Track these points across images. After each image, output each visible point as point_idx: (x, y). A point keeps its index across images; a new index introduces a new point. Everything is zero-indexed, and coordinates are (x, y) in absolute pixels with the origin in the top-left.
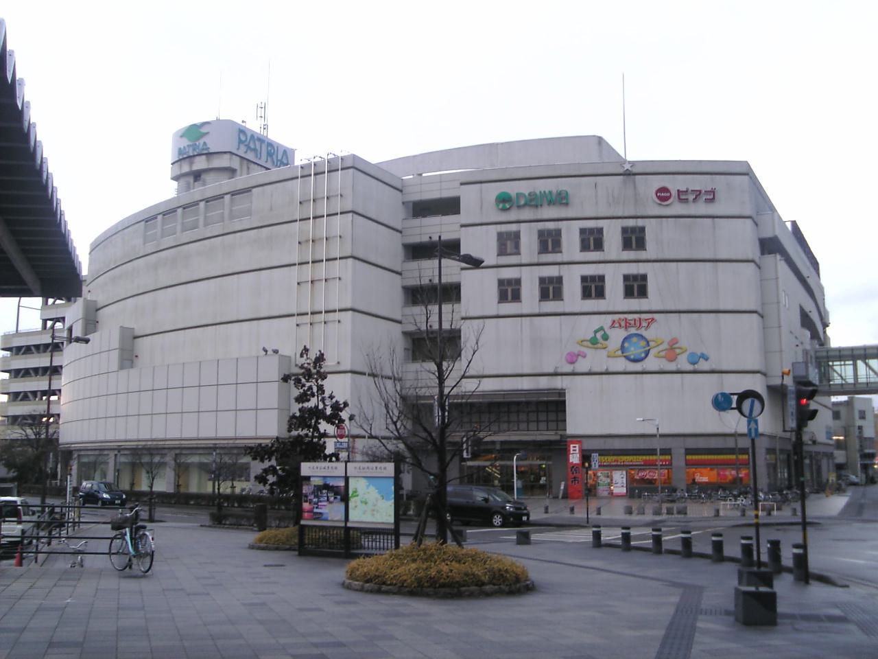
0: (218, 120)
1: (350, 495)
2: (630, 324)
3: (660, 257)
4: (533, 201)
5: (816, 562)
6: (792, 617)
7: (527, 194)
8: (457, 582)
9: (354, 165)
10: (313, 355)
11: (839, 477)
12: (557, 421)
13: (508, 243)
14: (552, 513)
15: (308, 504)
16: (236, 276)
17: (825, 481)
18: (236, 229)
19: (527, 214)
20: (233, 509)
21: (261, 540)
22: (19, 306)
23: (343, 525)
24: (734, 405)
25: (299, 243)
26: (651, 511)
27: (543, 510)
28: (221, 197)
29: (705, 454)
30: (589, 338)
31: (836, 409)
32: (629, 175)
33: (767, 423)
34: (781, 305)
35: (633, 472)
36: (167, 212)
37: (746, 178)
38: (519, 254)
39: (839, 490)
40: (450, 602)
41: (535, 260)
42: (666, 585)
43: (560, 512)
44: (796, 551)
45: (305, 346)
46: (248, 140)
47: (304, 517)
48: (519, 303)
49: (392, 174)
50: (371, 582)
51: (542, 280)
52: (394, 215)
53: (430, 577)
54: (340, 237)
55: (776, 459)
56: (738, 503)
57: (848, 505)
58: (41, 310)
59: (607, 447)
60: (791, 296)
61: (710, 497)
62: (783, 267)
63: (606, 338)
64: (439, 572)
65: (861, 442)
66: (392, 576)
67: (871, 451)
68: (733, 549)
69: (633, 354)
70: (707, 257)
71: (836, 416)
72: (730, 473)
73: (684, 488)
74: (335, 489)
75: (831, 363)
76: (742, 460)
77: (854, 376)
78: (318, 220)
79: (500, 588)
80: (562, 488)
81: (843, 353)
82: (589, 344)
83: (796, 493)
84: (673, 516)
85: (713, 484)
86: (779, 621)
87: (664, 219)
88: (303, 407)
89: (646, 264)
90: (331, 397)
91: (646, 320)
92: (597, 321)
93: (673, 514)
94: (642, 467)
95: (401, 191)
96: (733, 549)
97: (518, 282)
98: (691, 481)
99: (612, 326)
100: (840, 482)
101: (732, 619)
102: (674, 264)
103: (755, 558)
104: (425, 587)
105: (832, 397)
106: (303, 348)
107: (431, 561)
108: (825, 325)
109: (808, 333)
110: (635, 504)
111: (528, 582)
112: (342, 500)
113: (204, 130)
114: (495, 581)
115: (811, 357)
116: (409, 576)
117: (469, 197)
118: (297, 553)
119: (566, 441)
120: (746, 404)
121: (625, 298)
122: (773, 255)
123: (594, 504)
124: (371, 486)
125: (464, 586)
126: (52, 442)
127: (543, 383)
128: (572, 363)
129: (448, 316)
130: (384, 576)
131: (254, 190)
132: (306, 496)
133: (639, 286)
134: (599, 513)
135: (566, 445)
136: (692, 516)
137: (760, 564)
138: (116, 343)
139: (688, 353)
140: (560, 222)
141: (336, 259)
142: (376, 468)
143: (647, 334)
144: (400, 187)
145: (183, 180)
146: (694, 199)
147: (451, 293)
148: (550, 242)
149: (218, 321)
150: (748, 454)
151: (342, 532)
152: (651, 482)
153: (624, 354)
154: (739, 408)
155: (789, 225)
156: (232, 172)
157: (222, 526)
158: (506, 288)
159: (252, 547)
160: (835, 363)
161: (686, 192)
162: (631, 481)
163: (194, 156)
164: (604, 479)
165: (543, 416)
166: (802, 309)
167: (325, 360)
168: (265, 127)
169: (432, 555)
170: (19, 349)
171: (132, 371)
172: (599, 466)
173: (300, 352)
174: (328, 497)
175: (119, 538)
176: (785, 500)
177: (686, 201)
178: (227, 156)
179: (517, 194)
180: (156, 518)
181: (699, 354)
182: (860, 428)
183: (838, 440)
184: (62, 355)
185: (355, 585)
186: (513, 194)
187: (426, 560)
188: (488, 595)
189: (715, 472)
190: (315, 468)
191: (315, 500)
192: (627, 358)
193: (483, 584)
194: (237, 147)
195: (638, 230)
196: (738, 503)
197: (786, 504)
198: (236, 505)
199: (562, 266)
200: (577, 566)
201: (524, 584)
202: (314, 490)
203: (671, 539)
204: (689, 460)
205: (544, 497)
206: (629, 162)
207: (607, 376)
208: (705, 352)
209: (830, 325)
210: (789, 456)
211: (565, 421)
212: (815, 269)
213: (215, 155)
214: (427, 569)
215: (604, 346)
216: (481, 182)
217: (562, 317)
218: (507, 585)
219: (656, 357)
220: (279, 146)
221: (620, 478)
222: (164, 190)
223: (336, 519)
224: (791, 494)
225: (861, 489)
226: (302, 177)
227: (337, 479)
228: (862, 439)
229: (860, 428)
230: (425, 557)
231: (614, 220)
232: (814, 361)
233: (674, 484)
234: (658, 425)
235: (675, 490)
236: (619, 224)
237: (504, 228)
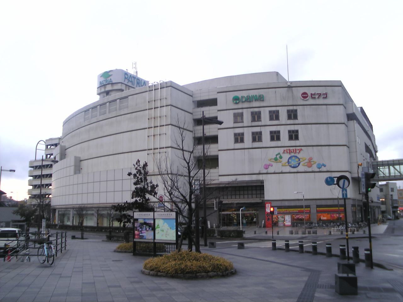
0: (116, 69)
1: (156, 227)
2: (291, 151)
3: (304, 122)
4: (249, 99)
5: (377, 256)
6: (365, 289)
7: (246, 97)
8: (195, 271)
9: (171, 86)
10: (142, 164)
11: (383, 217)
12: (261, 194)
13: (238, 117)
14: (258, 234)
15: (137, 231)
16: (122, 134)
17: (377, 218)
18: (122, 114)
19: (246, 105)
20: (120, 233)
21: (119, 248)
22: (36, 149)
23: (153, 241)
24: (335, 183)
25: (148, 119)
26: (301, 233)
27: (254, 233)
28: (115, 100)
29: (325, 207)
30: (274, 158)
31: (381, 187)
33: (351, 192)
34: (357, 142)
35: (294, 216)
36: (94, 107)
37: (340, 88)
38: (243, 122)
39: (383, 222)
40: (190, 281)
41: (250, 125)
42: (301, 270)
43: (261, 233)
44: (366, 252)
45: (138, 160)
46: (129, 77)
47: (135, 238)
48: (243, 144)
50: (154, 270)
51: (253, 133)
52: (190, 107)
53: (181, 269)
54: (166, 116)
55: (356, 209)
56: (340, 228)
57: (388, 229)
58: (45, 150)
59: (282, 205)
60: (360, 139)
61: (327, 226)
62: (357, 126)
63: (281, 158)
64: (186, 266)
65: (392, 201)
66: (163, 268)
67: (396, 205)
68: (336, 251)
69: (293, 165)
71: (381, 190)
72: (336, 216)
73: (316, 222)
75: (379, 168)
76: (341, 209)
77: (389, 173)
78: (156, 109)
79: (217, 274)
80: (263, 223)
81: (384, 163)
83: (365, 224)
84: (311, 235)
85: (329, 220)
86: (359, 291)
87: (305, 106)
88: (137, 187)
89: (298, 125)
90: (151, 183)
92: (277, 151)
93: (311, 234)
94: (297, 213)
95: (192, 96)
96: (336, 251)
97: (243, 134)
98: (319, 219)
99: (284, 153)
100: (384, 218)
101: (334, 290)
103: (347, 255)
104: (179, 273)
105: (379, 182)
106: (137, 160)
107: (183, 260)
108: (376, 152)
109: (369, 155)
110: (294, 230)
111: (233, 270)
112: (152, 229)
113: (110, 74)
114: (215, 270)
115: (370, 165)
116: (171, 268)
117: (221, 99)
118: (132, 254)
119: (264, 203)
120: (341, 182)
121: (289, 140)
122: (353, 121)
123: (276, 229)
124: (165, 223)
125: (199, 273)
126: (49, 205)
127: (254, 178)
128: (267, 169)
129: (212, 150)
130: (159, 268)
131: (129, 97)
132: (136, 228)
134: (278, 234)
135: (264, 204)
136: (319, 234)
137: (349, 258)
138: (73, 163)
139: (316, 164)
141: (164, 126)
142: (167, 214)
143: (299, 156)
144: (191, 95)
145: (102, 95)
146: (318, 97)
147: (214, 139)
148: (256, 117)
149: (115, 153)
151: (152, 244)
152: (302, 220)
153: (289, 165)
154: (338, 184)
155: (359, 109)
156: (122, 90)
157: (111, 241)
158: (237, 137)
159: (115, 251)
160: (380, 167)
162: (293, 219)
163: (106, 85)
164: (281, 219)
165: (254, 192)
166: (366, 144)
167: (148, 166)
168: (137, 73)
169: (184, 257)
170: (36, 167)
171: (79, 175)
172: (278, 213)
173: (136, 162)
174: (146, 228)
175: (41, 248)
176: (360, 227)
177: (315, 98)
178: (120, 84)
179: (242, 97)
180: (84, 237)
181: (322, 164)
182: (392, 195)
183: (382, 201)
184: (52, 169)
185: (146, 272)
186: (240, 96)
187: (181, 259)
188: (211, 277)
189: (329, 215)
190: (140, 215)
191: (140, 230)
192: (291, 166)
193: (209, 272)
195: (294, 111)
196: (340, 228)
197: (361, 228)
198: (121, 231)
199: (261, 127)
200: (260, 260)
201: (231, 271)
203: (308, 246)
204: (318, 210)
205: (256, 227)
206: (290, 82)
207: (282, 174)
208: (324, 163)
209: (378, 152)
210: (361, 208)
211: (264, 194)
212: (371, 128)
214: (180, 264)
215: (280, 161)
216: (226, 92)
217: (262, 149)
218: (221, 272)
219: (303, 165)
220: (142, 80)
221: (288, 218)
222: (94, 98)
223: (149, 238)
224: (363, 224)
225: (392, 222)
226: (149, 91)
227: (150, 220)
228: (392, 200)
229: (392, 195)
230: (181, 258)
231: (283, 107)
232: (371, 166)
233: (312, 220)
234: (304, 195)
235: (312, 223)
236: (286, 109)
237: (236, 111)
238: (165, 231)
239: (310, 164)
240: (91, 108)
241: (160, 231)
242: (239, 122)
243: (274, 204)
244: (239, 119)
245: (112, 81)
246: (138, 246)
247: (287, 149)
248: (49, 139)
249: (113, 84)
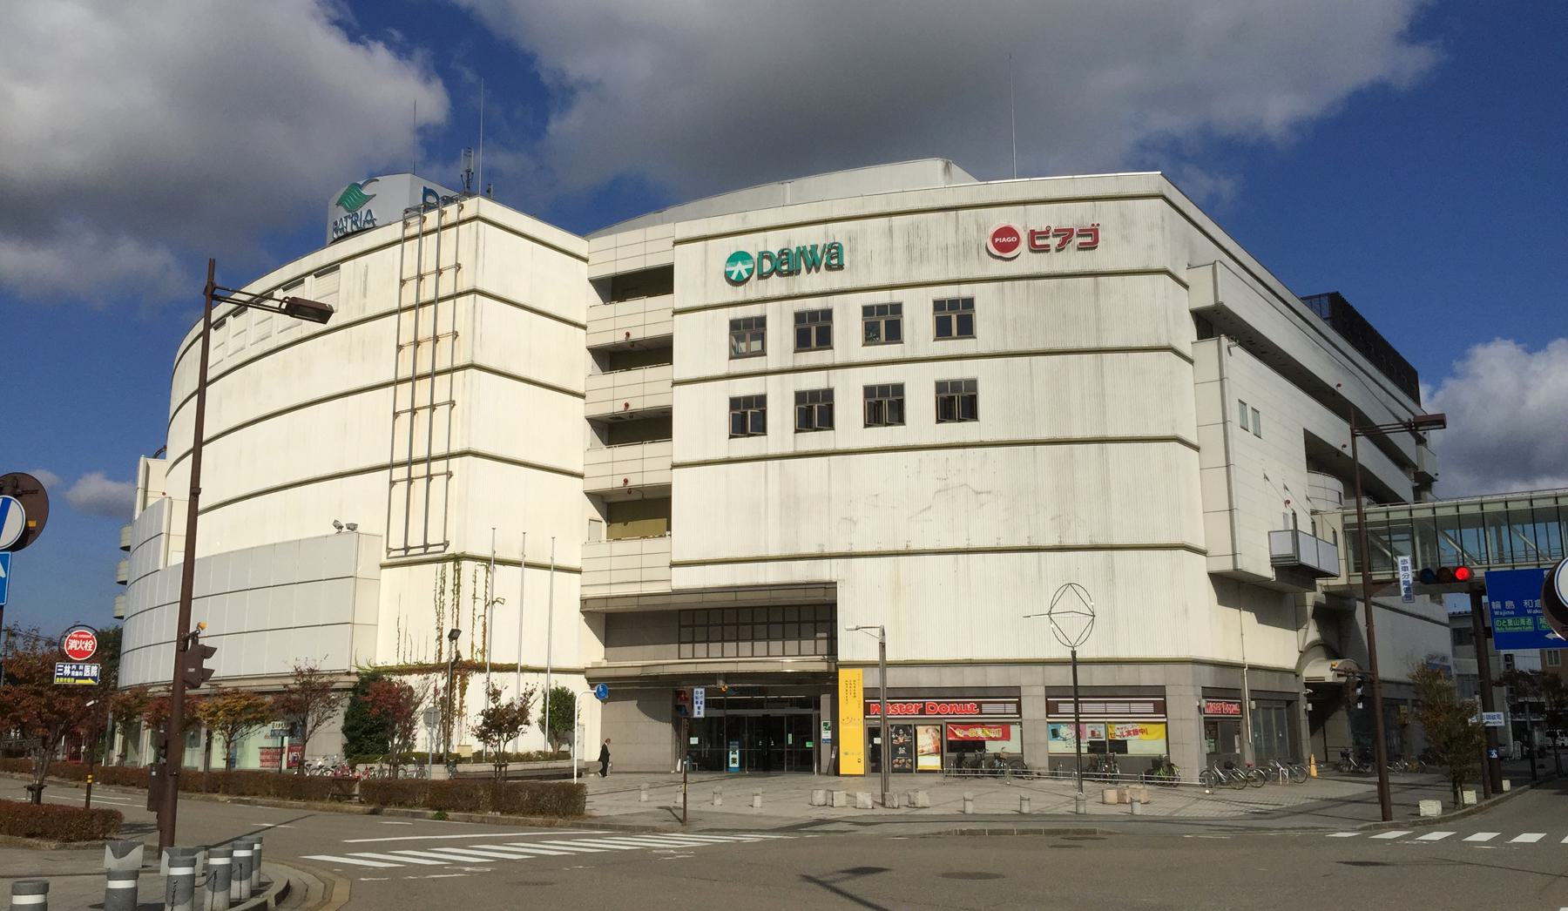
4: (786, 264)
13: (748, 333)
19: (776, 285)
41: (789, 364)
49: (318, 309)
70: (1085, 345)
87: (1006, 283)
97: (828, 394)
131: (343, 266)
161: (1045, 234)
177: (1045, 249)
216: (706, 238)
217: (832, 458)
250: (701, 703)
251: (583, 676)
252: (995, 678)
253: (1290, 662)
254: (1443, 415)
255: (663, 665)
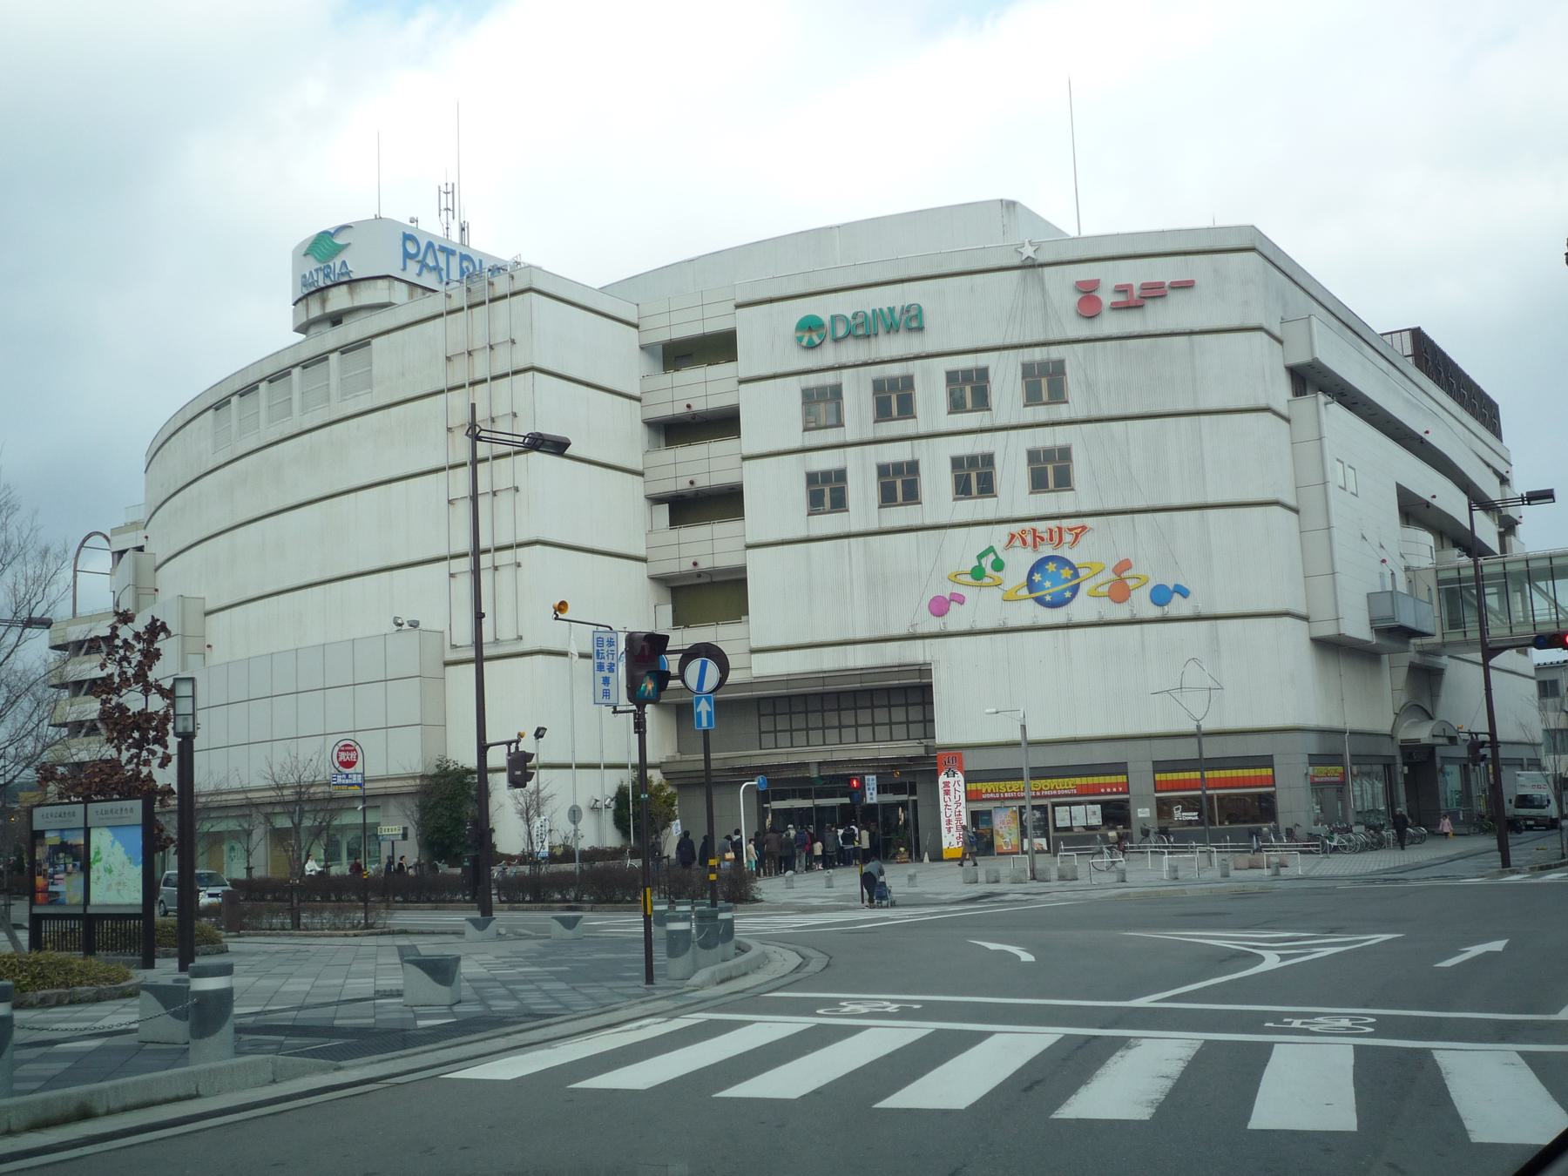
2: (1042, 539)
3: (1095, 414)
4: (863, 328)
7: (849, 316)
19: (852, 351)
30: (969, 569)
31: (1547, 676)
32: (1032, 266)
41: (869, 436)
63: (998, 565)
70: (1182, 408)
74: (74, 850)
82: (969, 579)
91: (1070, 530)
92: (980, 538)
97: (841, 475)
102: (1122, 424)
113: (339, 241)
127: (891, 655)
131: (375, 342)
132: (40, 865)
133: (1056, 469)
140: (910, 363)
144: (634, 320)
150: (1342, 764)
163: (328, 287)
181: (1171, 588)
186: (826, 319)
191: (50, 870)
192: (1040, 601)
194: (402, 267)
199: (916, 442)
202: (49, 853)
208: (1182, 583)
211: (933, 721)
213: (362, 283)
216: (771, 301)
237: (813, 381)
238: (116, 872)
239: (1119, 592)
240: (233, 394)
241: (102, 873)
242: (826, 427)
243: (973, 762)
244: (823, 410)
245: (348, 273)
246: (99, 933)
247: (1023, 531)
248: (126, 525)
249: (351, 283)
250: (873, 789)
251: (659, 771)
252: (1100, 755)
253: (1385, 726)
254: (1552, 490)
255: (750, 756)
